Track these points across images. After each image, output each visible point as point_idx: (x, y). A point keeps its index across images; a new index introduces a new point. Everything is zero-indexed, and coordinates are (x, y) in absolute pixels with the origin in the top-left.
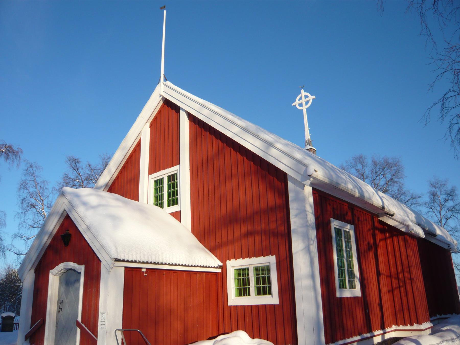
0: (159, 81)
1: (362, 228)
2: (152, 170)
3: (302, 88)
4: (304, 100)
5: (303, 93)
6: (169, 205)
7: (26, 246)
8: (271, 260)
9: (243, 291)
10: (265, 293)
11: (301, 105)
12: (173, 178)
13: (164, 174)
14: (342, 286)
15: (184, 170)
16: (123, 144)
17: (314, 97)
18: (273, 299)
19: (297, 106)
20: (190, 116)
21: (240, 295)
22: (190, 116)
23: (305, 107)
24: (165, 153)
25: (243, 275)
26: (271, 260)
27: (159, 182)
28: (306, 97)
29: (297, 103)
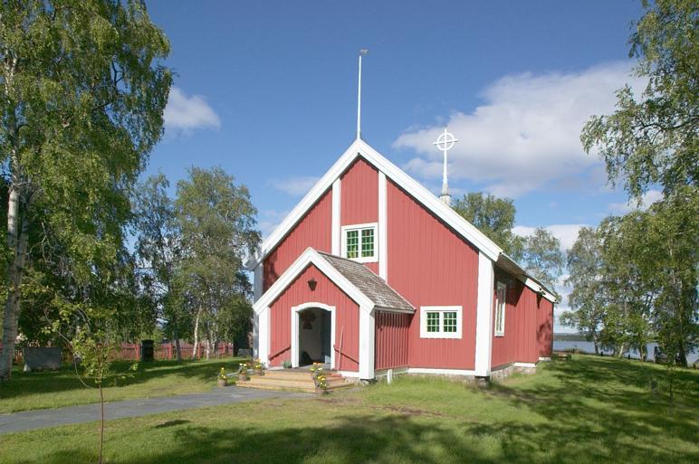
0: (355, 138)
2: (344, 222)
8: (459, 309)
10: (434, 330)
12: (368, 234)
18: (458, 335)
20: (387, 177)
22: (387, 177)
24: (360, 207)
26: (459, 309)
27: (352, 234)
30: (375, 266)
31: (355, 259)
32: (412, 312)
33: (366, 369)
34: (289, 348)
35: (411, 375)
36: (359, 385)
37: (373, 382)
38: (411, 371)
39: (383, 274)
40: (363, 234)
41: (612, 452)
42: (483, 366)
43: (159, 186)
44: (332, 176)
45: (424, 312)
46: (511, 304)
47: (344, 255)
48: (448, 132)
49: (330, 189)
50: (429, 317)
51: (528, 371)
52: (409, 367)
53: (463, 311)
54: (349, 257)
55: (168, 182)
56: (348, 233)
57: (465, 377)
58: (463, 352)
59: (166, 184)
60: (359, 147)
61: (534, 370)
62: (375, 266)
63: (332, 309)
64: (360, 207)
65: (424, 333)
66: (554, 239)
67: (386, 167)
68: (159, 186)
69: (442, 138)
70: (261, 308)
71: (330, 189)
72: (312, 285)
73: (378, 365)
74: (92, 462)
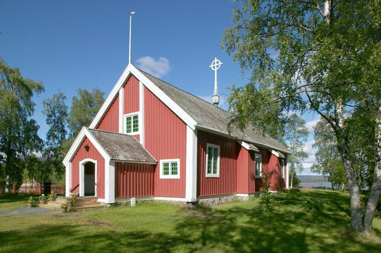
0: (128, 63)
1: (5, 207)
2: (125, 112)
3: (216, 56)
4: (216, 65)
5: (216, 60)
6: (134, 131)
7: (192, 233)
8: (178, 161)
9: (166, 173)
10: (167, 174)
11: (214, 67)
12: (136, 117)
13: (132, 115)
14: (209, 172)
15: (141, 114)
16: (108, 185)
17: (222, 63)
18: (178, 177)
19: (212, 68)
21: (165, 174)
23: (216, 69)
24: (132, 105)
25: (166, 165)
26: (178, 161)
27: (129, 119)
28: (218, 62)
29: (212, 66)
30: (138, 136)
31: (129, 134)
32: (155, 164)
33: (108, 197)
34: (78, 185)
35: (156, 200)
36: (106, 207)
37: (115, 205)
38: (156, 198)
39: (142, 141)
40: (134, 119)
41: (206, 240)
42: (190, 194)
43: (61, 100)
44: (118, 87)
45: (162, 162)
46: (229, 157)
47: (125, 133)
48: (217, 59)
49: (117, 96)
50: (165, 166)
51: (244, 199)
52: (155, 196)
53: (162, 159)
54: (128, 131)
55: (65, 97)
56: (127, 118)
57: (181, 202)
58: (178, 188)
59: (64, 98)
60: (131, 69)
61: (248, 198)
62: (138, 136)
63: (95, 162)
64: (132, 105)
65: (162, 176)
66: (302, 120)
67: (144, 80)
68: (61, 100)
69: (214, 63)
70: (66, 162)
71: (117, 96)
72: (87, 148)
73: (117, 195)
74: (27, 252)
